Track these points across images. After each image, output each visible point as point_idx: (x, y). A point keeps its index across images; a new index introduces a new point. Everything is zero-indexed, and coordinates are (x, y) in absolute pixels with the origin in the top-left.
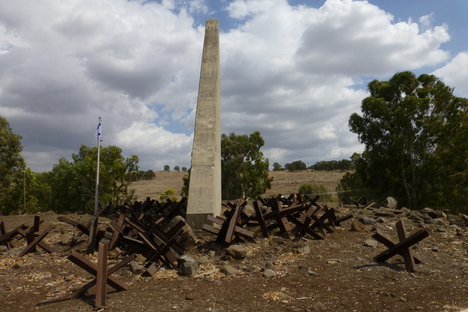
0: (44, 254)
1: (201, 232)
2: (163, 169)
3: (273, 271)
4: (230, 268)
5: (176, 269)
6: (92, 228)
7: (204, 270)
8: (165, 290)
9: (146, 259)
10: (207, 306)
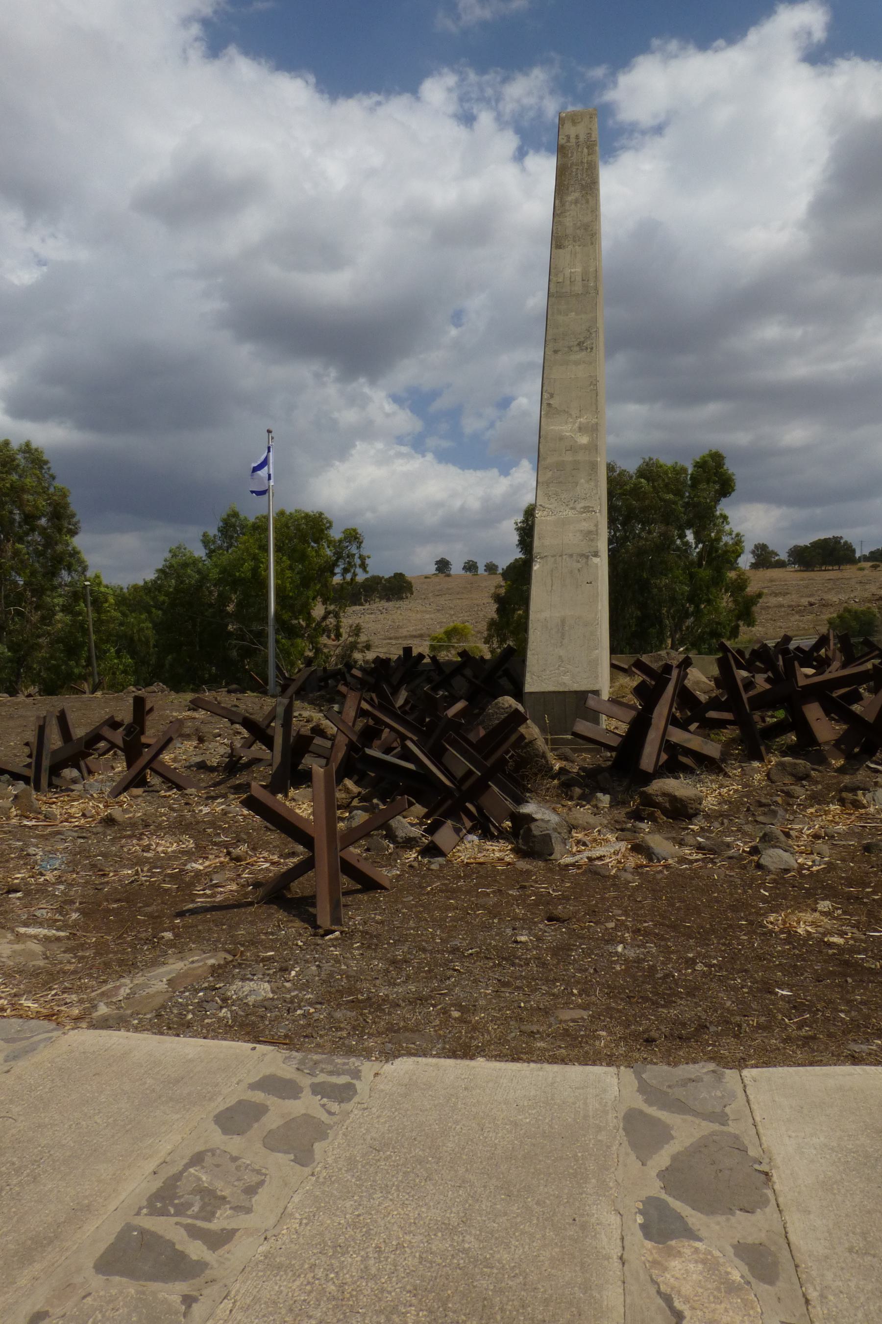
0: (166, 791)
1: (566, 742)
2: (432, 569)
3: (786, 855)
4: (659, 843)
5: (507, 839)
6: (277, 726)
7: (585, 844)
8: (488, 894)
9: (426, 810)
10: (611, 940)
